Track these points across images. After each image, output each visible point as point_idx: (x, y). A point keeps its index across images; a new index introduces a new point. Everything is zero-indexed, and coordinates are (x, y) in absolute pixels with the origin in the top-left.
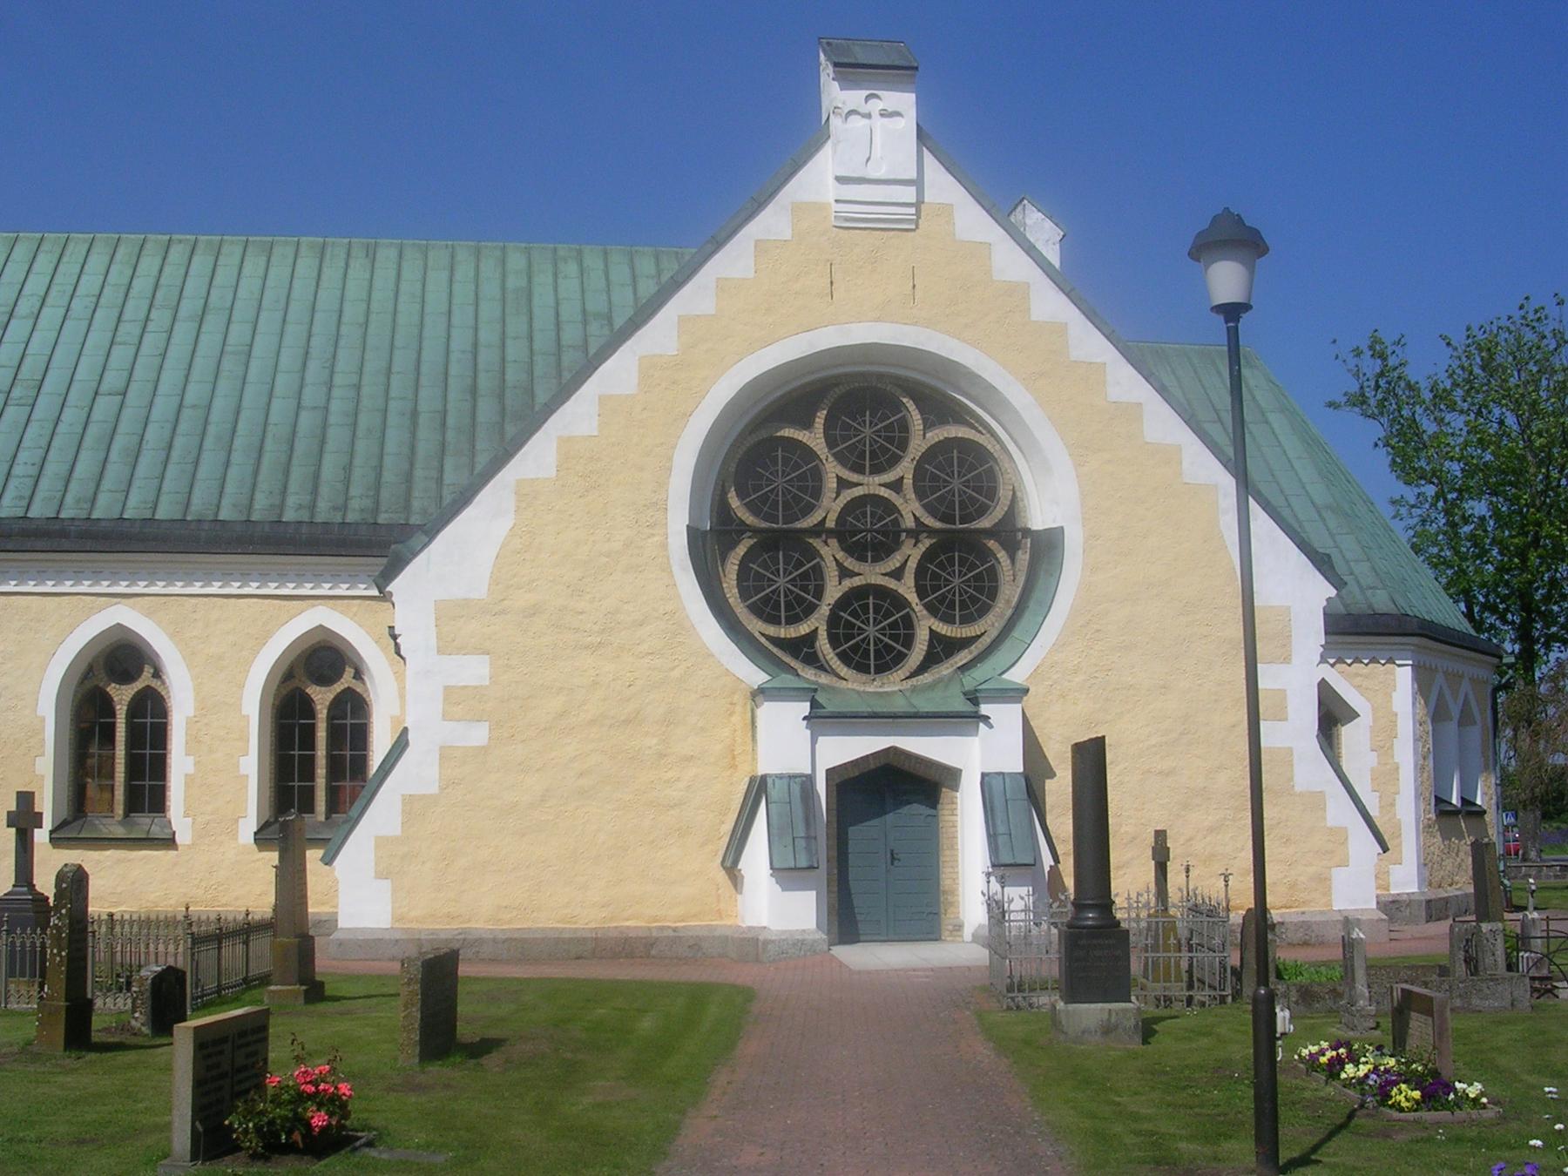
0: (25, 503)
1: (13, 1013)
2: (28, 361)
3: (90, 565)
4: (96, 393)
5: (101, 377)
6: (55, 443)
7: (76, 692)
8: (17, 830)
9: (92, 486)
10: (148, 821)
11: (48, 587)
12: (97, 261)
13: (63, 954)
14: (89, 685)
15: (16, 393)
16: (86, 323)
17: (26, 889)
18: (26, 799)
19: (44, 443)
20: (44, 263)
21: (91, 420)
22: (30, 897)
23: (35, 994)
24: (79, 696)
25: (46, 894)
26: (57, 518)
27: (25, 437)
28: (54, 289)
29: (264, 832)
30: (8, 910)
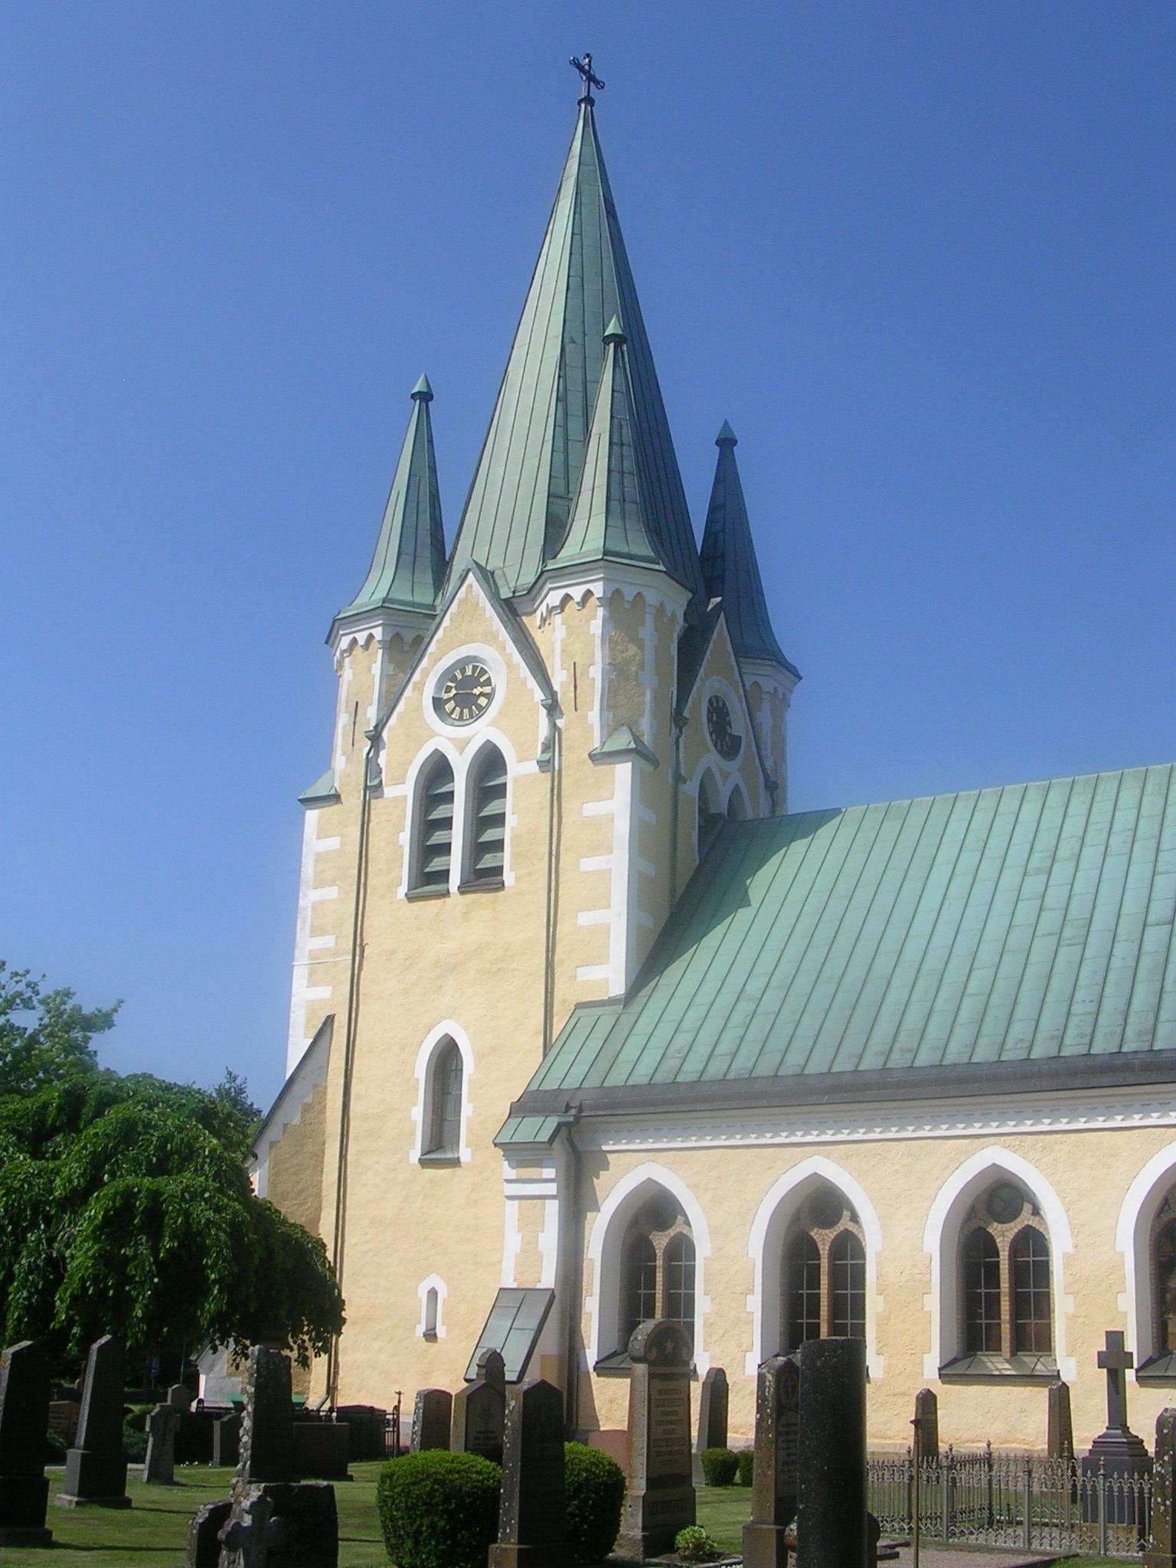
0: (1087, 1040)
1: (1112, 1561)
2: (1074, 902)
3: (1155, 1096)
4: (1145, 925)
5: (1148, 908)
6: (1110, 978)
7: (1153, 1226)
8: (1108, 1371)
9: (1152, 1016)
10: (1035, 1360)
11: (1118, 1121)
12: (1129, 796)
13: (1168, 1503)
14: (973, 1225)
15: (1067, 934)
16: (1126, 857)
17: (1120, 1432)
18: (1115, 1339)
19: (1100, 979)
20: (1078, 805)
21: (1143, 951)
22: (1125, 1440)
23: (1134, 1541)
24: (1157, 1230)
25: (1140, 1437)
26: (1120, 1052)
27: (1080, 974)
28: (1092, 828)
29: (948, 1369)
30: (1105, 1453)
